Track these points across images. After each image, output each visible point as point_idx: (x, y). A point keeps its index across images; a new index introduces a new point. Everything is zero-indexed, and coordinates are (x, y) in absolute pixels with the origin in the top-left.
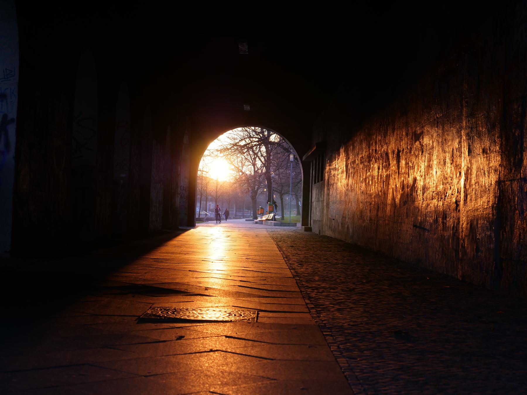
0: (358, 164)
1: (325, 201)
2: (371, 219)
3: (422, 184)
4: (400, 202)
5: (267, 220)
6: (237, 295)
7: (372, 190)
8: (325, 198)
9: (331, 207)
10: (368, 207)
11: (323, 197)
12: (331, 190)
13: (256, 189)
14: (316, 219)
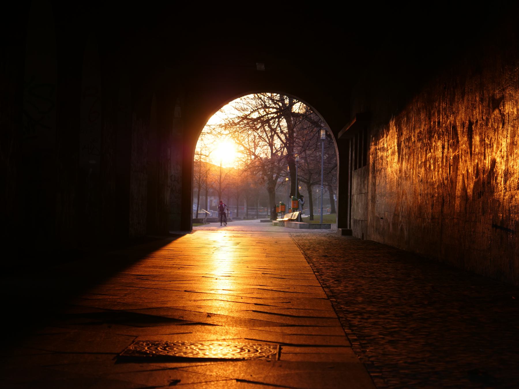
0: (415, 141)
1: (370, 194)
2: (433, 218)
3: (503, 168)
4: (473, 193)
5: (290, 220)
6: (251, 323)
7: (435, 177)
8: (370, 189)
9: (378, 201)
10: (429, 200)
11: (366, 187)
12: (377, 178)
13: (274, 179)
14: (358, 219)
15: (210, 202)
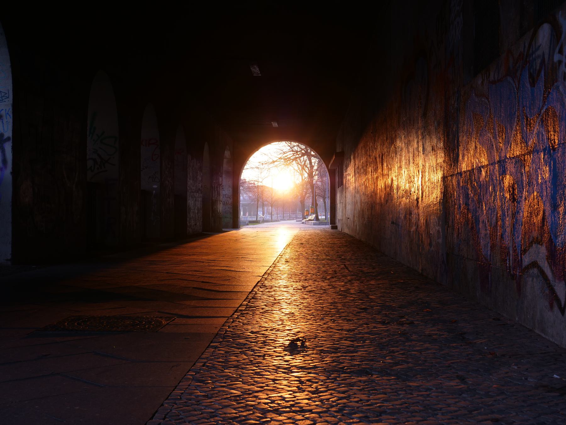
1: (344, 203)
3: (396, 183)
12: (347, 192)
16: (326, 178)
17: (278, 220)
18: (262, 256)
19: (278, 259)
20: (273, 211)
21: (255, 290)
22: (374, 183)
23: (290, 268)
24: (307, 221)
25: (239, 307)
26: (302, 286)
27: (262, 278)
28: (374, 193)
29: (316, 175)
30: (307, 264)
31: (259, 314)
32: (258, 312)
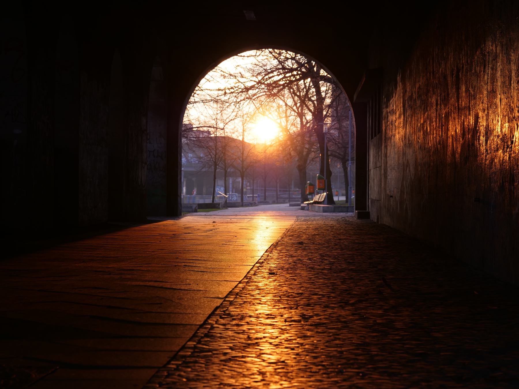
1: (383, 167)
4: (461, 159)
9: (389, 176)
11: (380, 160)
12: (388, 147)
14: (374, 199)
15: (232, 183)
16: (348, 122)
17: (255, 203)
18: (223, 263)
19: (255, 269)
20: (244, 186)
21: (210, 322)
22: (442, 126)
23: (278, 284)
24: (310, 204)
25: (179, 351)
26: (301, 316)
27: (224, 301)
28: (443, 144)
29: (328, 116)
30: (311, 278)
31: (218, 364)
32: (216, 360)
